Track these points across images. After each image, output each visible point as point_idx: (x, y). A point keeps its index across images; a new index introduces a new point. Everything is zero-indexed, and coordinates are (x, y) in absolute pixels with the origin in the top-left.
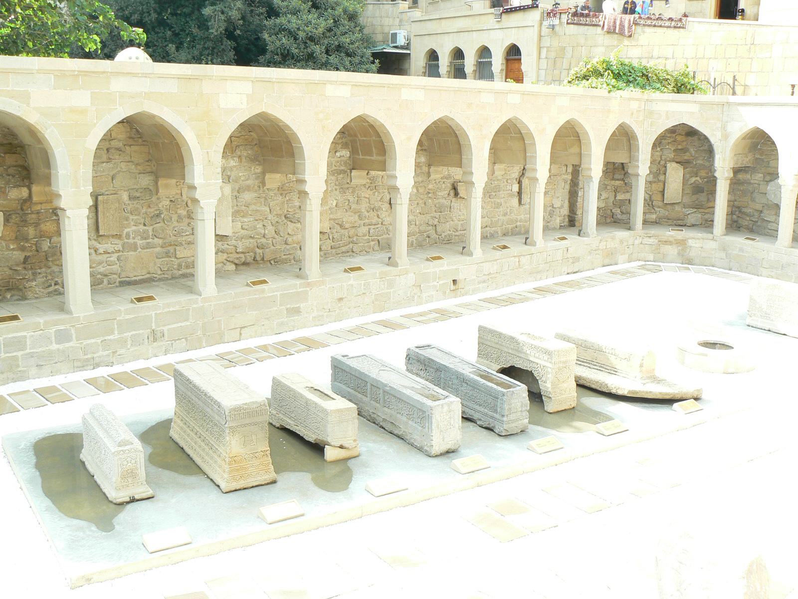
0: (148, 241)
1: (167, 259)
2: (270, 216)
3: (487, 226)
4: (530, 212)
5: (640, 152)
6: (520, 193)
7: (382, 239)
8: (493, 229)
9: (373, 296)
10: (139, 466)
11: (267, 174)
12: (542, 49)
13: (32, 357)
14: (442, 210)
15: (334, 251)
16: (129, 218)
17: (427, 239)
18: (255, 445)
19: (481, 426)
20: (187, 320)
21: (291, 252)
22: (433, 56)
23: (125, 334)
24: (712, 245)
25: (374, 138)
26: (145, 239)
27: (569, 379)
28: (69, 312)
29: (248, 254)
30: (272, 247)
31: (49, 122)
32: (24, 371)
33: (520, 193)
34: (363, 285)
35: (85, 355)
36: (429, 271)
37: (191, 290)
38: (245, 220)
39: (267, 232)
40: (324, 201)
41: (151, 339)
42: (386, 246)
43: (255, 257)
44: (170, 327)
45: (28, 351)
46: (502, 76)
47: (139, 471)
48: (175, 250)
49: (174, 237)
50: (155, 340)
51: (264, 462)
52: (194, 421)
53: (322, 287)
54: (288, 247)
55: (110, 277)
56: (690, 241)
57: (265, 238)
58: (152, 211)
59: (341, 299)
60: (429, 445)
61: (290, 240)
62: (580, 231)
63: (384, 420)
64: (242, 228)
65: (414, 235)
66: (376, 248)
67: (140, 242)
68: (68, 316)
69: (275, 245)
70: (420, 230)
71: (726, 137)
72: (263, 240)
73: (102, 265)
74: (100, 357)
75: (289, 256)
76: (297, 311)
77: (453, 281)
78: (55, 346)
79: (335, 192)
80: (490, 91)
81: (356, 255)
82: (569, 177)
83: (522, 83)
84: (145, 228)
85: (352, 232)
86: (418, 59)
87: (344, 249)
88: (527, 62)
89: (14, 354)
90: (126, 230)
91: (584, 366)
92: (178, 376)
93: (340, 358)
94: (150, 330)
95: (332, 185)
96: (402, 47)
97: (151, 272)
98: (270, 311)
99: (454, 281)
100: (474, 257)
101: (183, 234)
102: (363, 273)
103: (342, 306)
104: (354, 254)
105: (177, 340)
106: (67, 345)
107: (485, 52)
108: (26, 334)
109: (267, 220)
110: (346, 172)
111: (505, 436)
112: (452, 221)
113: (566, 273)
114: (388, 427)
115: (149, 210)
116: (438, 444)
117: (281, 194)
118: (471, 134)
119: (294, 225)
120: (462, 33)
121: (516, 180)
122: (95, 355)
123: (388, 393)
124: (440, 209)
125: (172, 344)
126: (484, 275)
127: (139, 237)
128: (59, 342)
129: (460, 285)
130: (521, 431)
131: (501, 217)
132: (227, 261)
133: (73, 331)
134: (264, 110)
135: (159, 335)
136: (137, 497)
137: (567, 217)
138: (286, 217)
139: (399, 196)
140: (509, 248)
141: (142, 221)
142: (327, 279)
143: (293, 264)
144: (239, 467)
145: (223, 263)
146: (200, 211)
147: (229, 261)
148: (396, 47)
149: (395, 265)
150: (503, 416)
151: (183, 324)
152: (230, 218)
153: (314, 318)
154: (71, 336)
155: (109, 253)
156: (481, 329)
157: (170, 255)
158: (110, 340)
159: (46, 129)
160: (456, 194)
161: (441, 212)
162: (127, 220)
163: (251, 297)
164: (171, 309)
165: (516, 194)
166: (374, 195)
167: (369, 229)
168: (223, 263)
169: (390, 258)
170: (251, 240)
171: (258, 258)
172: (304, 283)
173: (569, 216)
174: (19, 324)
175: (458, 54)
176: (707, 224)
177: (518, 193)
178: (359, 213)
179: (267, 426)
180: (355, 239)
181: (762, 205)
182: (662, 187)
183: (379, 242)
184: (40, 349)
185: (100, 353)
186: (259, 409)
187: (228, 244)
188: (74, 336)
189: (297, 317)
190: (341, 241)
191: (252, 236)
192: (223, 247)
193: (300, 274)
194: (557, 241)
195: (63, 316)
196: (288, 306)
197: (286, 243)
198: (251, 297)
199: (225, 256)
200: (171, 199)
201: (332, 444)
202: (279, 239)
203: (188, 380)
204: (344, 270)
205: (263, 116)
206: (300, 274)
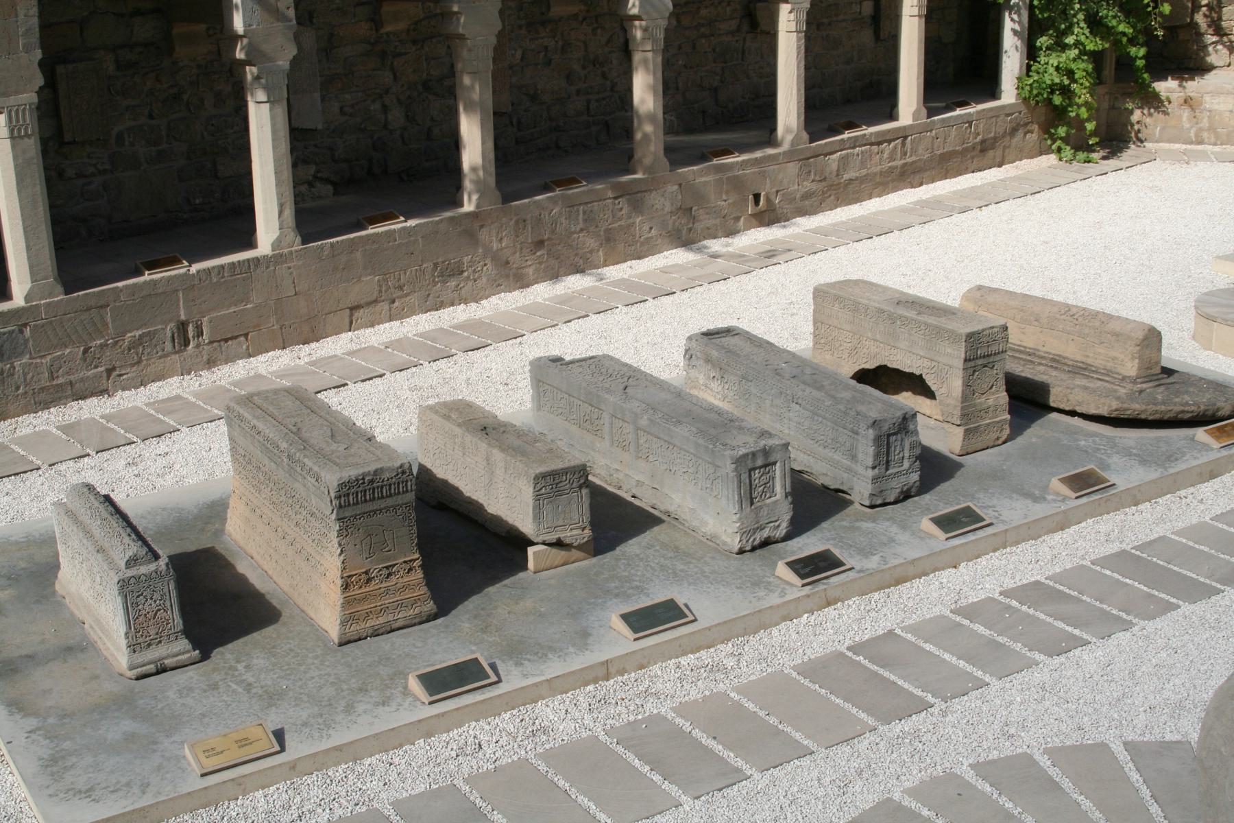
0: (160, 148)
52: (271, 507)
74: (82, 380)
152: (317, 95)
155: (86, 176)
187: (316, 146)
190: (535, 127)
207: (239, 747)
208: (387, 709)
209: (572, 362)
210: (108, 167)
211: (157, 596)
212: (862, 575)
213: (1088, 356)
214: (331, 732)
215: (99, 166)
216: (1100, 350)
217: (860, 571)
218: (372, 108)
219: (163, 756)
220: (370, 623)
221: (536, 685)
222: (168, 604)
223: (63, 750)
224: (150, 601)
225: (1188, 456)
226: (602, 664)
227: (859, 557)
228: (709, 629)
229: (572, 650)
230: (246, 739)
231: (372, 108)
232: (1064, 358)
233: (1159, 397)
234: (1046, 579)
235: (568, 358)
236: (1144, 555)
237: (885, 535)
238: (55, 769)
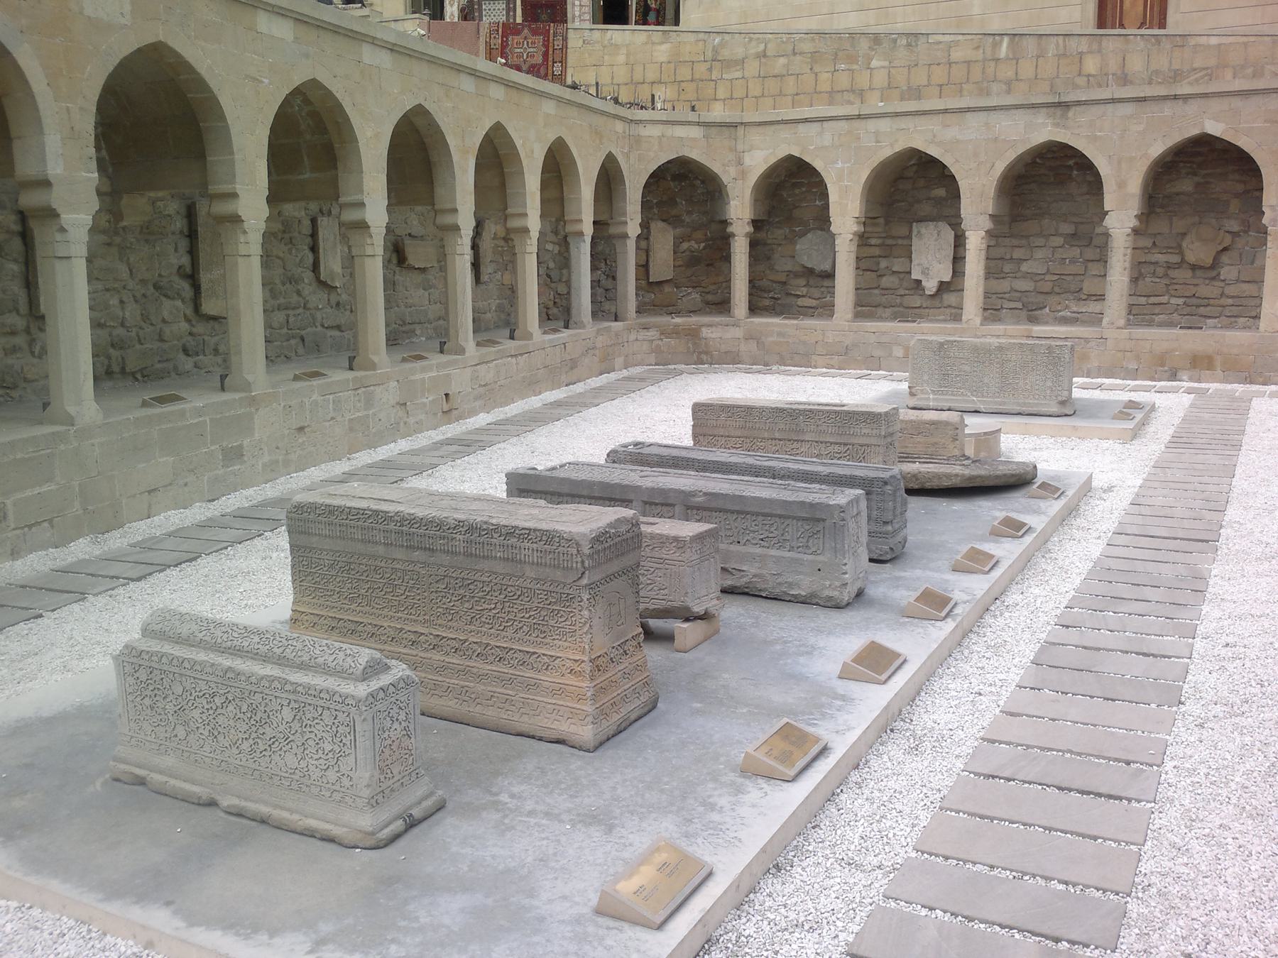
2: (131, 284)
3: (439, 319)
9: (346, 423)
11: (124, 195)
24: (738, 333)
25: (308, 137)
30: (138, 346)
34: (331, 401)
39: (127, 314)
44: (19, 496)
54: (166, 346)
56: (704, 330)
59: (301, 429)
66: (301, 350)
71: (743, 174)
72: (120, 331)
83: (420, 111)
98: (196, 455)
102: (326, 380)
109: (126, 291)
112: (398, 306)
117: (147, 241)
119: (172, 302)
126: (481, 386)
134: (161, 38)
136: (417, 812)
138: (157, 287)
139: (369, 241)
140: (498, 343)
151: (45, 488)
166: (290, 254)
167: (288, 316)
171: (116, 368)
172: (241, 398)
174: (662, 52)
176: (722, 305)
179: (1090, 471)
181: (785, 274)
182: (645, 258)
189: (239, 467)
191: (102, 321)
197: (161, 340)
202: (149, 329)
204: (292, 377)
231: (111, 303)
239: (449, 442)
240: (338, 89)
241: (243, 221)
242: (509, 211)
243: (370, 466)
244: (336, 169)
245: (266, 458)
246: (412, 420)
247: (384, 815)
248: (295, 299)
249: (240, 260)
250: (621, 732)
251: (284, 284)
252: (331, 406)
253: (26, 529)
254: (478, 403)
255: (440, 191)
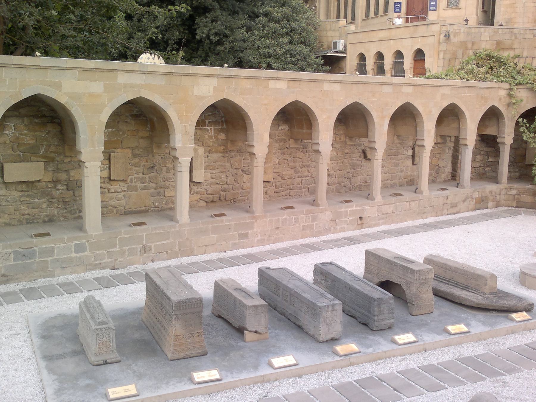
0: (145, 185)
1: (159, 197)
3: (388, 180)
4: (419, 171)
5: (506, 127)
6: (413, 156)
7: (311, 187)
8: (393, 181)
10: (111, 340)
12: (440, 52)
13: (58, 261)
14: (355, 168)
15: (276, 194)
16: (132, 169)
17: (344, 188)
18: (193, 328)
19: (360, 323)
20: (168, 239)
21: (245, 195)
22: (362, 57)
23: (124, 248)
26: (143, 183)
27: (428, 292)
28: (85, 232)
29: (215, 195)
30: (232, 191)
31: (75, 103)
32: (51, 271)
33: (413, 156)
34: (293, 219)
35: (95, 261)
36: (342, 210)
37: (172, 219)
38: (214, 172)
39: (228, 180)
40: (267, 160)
41: (142, 251)
42: (313, 191)
43: (220, 198)
44: (156, 244)
45: (55, 257)
46: (411, 72)
47: (111, 343)
48: (164, 191)
49: (163, 183)
50: (145, 252)
51: (184, 343)
52: (156, 310)
53: (264, 219)
54: (243, 191)
55: (118, 208)
57: (227, 184)
58: (149, 164)
59: (278, 228)
60: (318, 334)
61: (245, 186)
62: (458, 184)
63: (291, 314)
64: (212, 178)
65: (335, 185)
66: (307, 193)
67: (139, 185)
68: (84, 234)
69: (234, 190)
70: (338, 181)
72: (226, 186)
73: (113, 200)
74: (105, 263)
75: (244, 197)
76: (246, 236)
77: (360, 217)
78: (74, 255)
79: (278, 154)
80: (330, 81)
81: (292, 198)
82: (453, 145)
84: (144, 176)
85: (289, 181)
86: (351, 62)
87: (283, 193)
88: (429, 63)
89: (46, 259)
90: (130, 177)
91: (444, 283)
92: (148, 278)
93: (264, 269)
94: (141, 246)
95: (276, 148)
96: (341, 52)
97: (147, 206)
98: (227, 235)
99: (361, 218)
100: (376, 201)
101: (169, 181)
103: (278, 233)
104: (290, 197)
105: (161, 253)
106: (83, 254)
107: (399, 54)
108: (54, 246)
110: (286, 140)
111: (376, 330)
113: (446, 214)
114: (293, 319)
115: (147, 164)
116: (324, 333)
118: (374, 114)
119: (248, 176)
120: (383, 41)
121: (411, 147)
122: (102, 262)
123: (293, 295)
124: (354, 167)
125: (157, 255)
126: (383, 214)
127: (139, 182)
128: (77, 251)
129: (364, 220)
130: (389, 328)
131: (399, 173)
132: (200, 199)
133: (87, 244)
134: (225, 97)
135: (147, 249)
136: (108, 361)
137: (450, 174)
139: (321, 157)
141: (142, 171)
142: (268, 214)
143: (247, 203)
144: (181, 343)
145: (197, 201)
146: (179, 165)
147: (202, 200)
148: (337, 52)
149: (318, 205)
150: (374, 316)
151: (166, 242)
152: (203, 171)
153: (258, 240)
154: (86, 248)
155: (118, 192)
156: (368, 253)
157: (160, 194)
158: (113, 251)
159: (73, 107)
160: (365, 157)
161: (354, 169)
162: (131, 170)
163: (214, 225)
164: (157, 232)
165: (411, 157)
166: (306, 156)
168: (197, 201)
169: (314, 201)
170: (218, 186)
171: (222, 198)
173: (452, 173)
175: (380, 56)
177: (412, 156)
178: (294, 169)
180: (291, 186)
183: (309, 189)
184: (64, 256)
185: (106, 260)
186: (196, 303)
187: (201, 188)
188: (88, 248)
190: (281, 188)
191: (218, 183)
192: (197, 190)
193: (248, 210)
194: (440, 190)
195: (81, 234)
196: (240, 232)
198: (214, 225)
199: (199, 196)
200: (162, 157)
201: (250, 329)
203: (153, 281)
205: (225, 101)
206: (248, 210)
207: (125, 392)
208: (181, 384)
209: (273, 269)
210: (126, 189)
211: (107, 336)
212: (364, 354)
213: (469, 283)
214: (159, 390)
215: (122, 189)
216: (473, 281)
217: (364, 353)
218: (222, 177)
219: (98, 393)
220: (183, 354)
221: (236, 381)
222: (111, 340)
223: (64, 387)
224: (104, 338)
225: (503, 324)
226: (262, 376)
227: (365, 348)
228: (303, 368)
229: (252, 370)
230: (127, 389)
231: (222, 177)
232: (460, 283)
233: (494, 300)
234: (57, 284)
235: (272, 268)
236: (514, 364)
237: (377, 341)
238: (59, 394)
239: (346, 239)
240: (309, 102)
241: (255, 155)
242: (418, 137)
243: (460, 218)
244: (312, 130)
245: (259, 238)
246: (338, 227)
247: (98, 359)
248: (306, 173)
249: (254, 168)
250: (185, 358)
251: (301, 168)
252: (293, 220)
253: (158, 254)
254: (381, 221)
255: (370, 134)
